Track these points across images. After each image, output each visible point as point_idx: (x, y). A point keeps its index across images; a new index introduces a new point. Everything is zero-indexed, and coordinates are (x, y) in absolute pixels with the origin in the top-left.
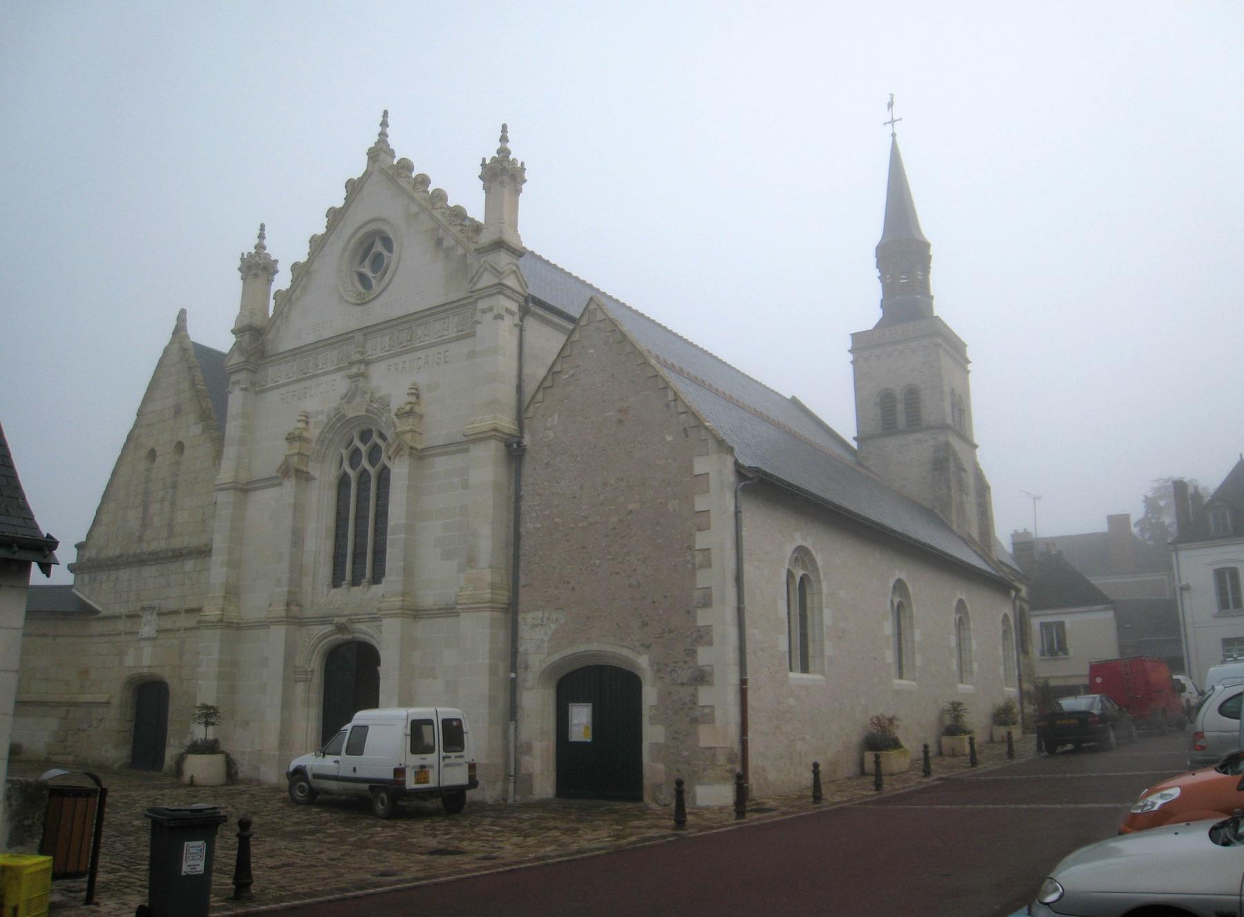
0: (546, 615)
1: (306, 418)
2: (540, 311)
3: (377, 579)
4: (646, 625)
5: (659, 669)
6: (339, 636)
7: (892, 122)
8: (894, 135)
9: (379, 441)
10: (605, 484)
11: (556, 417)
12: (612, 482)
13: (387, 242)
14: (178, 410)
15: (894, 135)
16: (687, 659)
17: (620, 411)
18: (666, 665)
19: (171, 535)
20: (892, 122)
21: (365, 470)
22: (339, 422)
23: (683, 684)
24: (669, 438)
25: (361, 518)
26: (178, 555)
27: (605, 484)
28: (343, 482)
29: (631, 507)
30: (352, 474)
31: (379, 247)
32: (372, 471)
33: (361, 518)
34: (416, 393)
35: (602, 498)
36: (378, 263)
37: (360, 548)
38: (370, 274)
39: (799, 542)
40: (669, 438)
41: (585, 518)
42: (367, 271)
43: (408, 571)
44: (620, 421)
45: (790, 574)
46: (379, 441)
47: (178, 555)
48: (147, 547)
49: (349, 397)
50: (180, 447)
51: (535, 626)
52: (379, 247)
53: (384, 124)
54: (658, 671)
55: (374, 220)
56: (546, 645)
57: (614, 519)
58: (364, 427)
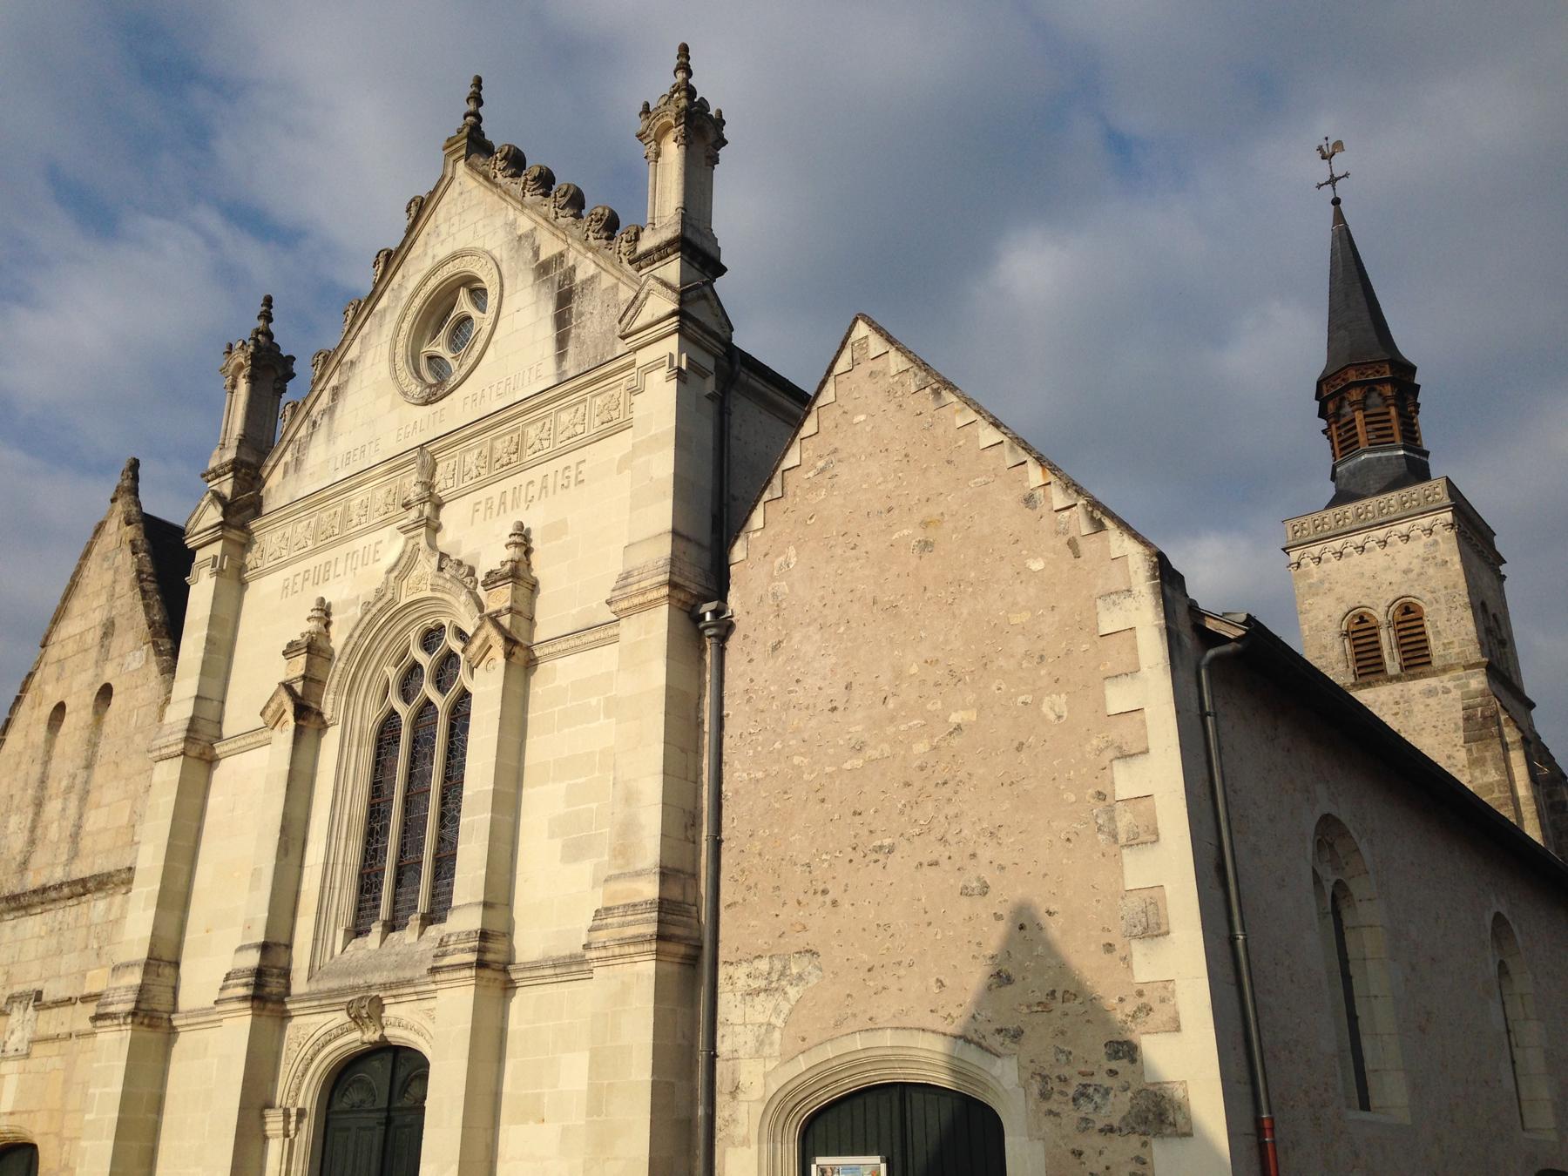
0: (778, 965)
1: (324, 612)
2: (757, 384)
3: (434, 916)
4: (1009, 980)
5: (1045, 1086)
6: (357, 1035)
7: (1333, 181)
8: (1336, 202)
9: (457, 646)
10: (899, 674)
11: (792, 551)
12: (914, 670)
13: (479, 295)
14: (109, 629)
15: (1336, 202)
16: (1114, 1065)
17: (925, 524)
18: (1063, 1080)
19: (74, 855)
20: (1333, 181)
21: (428, 703)
22: (383, 613)
23: (1110, 1130)
24: (1037, 565)
25: (414, 801)
26: (82, 888)
27: (899, 674)
28: (387, 730)
29: (955, 718)
30: (405, 712)
31: (464, 305)
32: (441, 702)
33: (414, 801)
34: (523, 539)
35: (891, 704)
36: (461, 331)
37: (407, 843)
38: (448, 355)
39: (1324, 807)
40: (1037, 565)
41: (859, 748)
42: (440, 348)
43: (498, 898)
44: (926, 545)
45: (1317, 880)
46: (457, 646)
47: (82, 888)
48: (33, 881)
49: (403, 568)
50: (106, 692)
51: (754, 993)
52: (464, 305)
53: (477, 99)
54: (1045, 1096)
55: (454, 257)
56: (777, 1035)
57: (921, 747)
58: (429, 622)
